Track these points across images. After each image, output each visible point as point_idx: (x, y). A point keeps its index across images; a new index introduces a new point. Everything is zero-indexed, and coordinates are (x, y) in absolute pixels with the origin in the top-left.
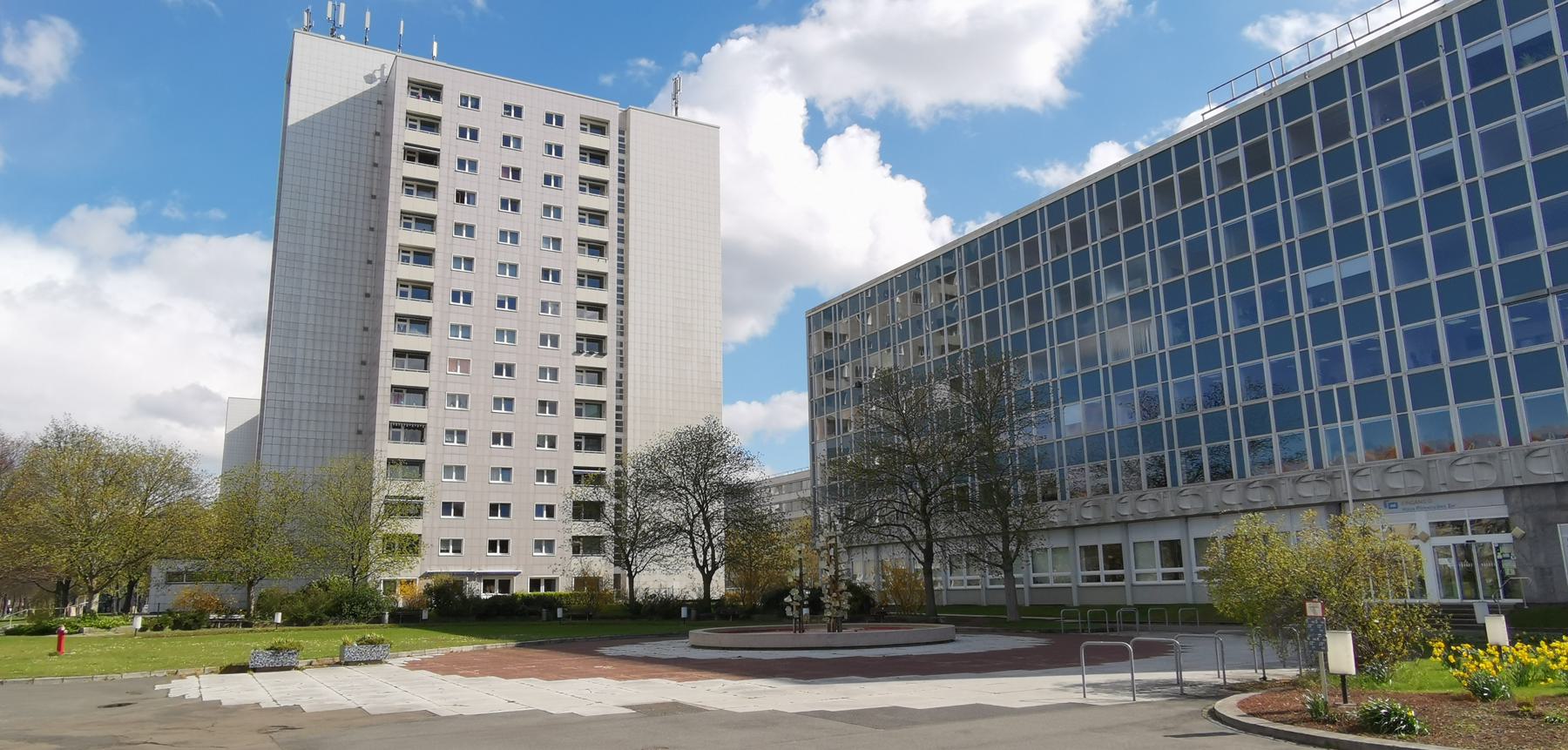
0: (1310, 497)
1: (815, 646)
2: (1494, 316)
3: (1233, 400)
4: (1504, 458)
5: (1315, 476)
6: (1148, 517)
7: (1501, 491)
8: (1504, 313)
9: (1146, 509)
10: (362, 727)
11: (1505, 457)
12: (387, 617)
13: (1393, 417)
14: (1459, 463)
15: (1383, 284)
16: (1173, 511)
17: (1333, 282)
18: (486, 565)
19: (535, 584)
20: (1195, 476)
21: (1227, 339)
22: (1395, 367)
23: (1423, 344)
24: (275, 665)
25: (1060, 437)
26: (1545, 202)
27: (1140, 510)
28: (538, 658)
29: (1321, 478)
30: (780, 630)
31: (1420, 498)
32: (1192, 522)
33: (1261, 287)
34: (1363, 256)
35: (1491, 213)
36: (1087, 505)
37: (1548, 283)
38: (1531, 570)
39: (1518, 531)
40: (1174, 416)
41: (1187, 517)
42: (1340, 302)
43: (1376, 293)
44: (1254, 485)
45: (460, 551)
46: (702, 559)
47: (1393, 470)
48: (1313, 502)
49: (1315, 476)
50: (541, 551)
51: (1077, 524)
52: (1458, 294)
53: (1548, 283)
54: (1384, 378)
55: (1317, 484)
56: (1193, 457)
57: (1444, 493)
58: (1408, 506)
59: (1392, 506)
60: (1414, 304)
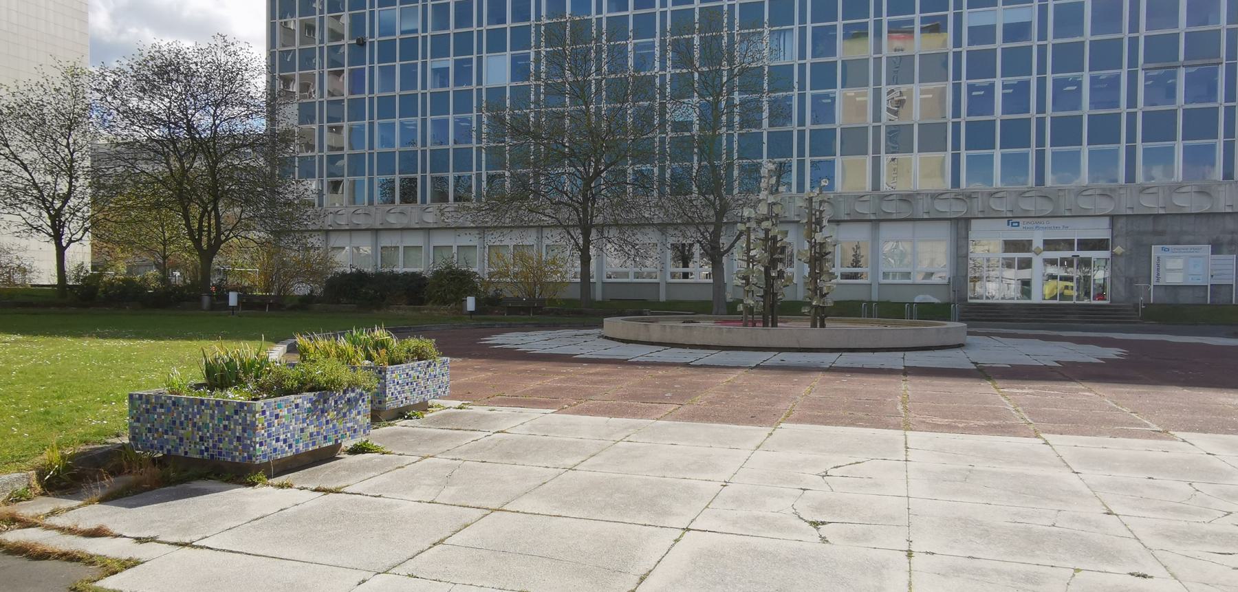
0: (867, 214)
1: (716, 343)
2: (1133, 77)
3: (424, 143)
4: (1121, 192)
5: (954, 194)
6: (395, 227)
7: (947, 225)
8: (1141, 76)
9: (393, 220)
10: (181, 545)
11: (1122, 192)
13: (1032, 152)
14: (1085, 193)
15: (1042, 35)
16: (382, 224)
17: (449, 68)
20: (441, 197)
21: (371, 99)
22: (1041, 108)
23: (1066, 95)
25: (373, 149)
26: (925, 17)
28: (683, 376)
29: (959, 197)
30: (1051, 321)
31: (1040, 220)
33: (455, 60)
34: (503, 55)
36: (358, 212)
37: (1181, 57)
38: (1124, 279)
39: (1118, 250)
40: (429, 147)
42: (999, 45)
43: (1035, 43)
44: (890, 198)
46: (197, 226)
48: (343, 228)
49: (954, 194)
52: (1106, 55)
53: (1181, 57)
54: (835, 127)
55: (954, 202)
56: (440, 182)
57: (1068, 216)
58: (1029, 226)
59: (1014, 224)
60: (1067, 58)
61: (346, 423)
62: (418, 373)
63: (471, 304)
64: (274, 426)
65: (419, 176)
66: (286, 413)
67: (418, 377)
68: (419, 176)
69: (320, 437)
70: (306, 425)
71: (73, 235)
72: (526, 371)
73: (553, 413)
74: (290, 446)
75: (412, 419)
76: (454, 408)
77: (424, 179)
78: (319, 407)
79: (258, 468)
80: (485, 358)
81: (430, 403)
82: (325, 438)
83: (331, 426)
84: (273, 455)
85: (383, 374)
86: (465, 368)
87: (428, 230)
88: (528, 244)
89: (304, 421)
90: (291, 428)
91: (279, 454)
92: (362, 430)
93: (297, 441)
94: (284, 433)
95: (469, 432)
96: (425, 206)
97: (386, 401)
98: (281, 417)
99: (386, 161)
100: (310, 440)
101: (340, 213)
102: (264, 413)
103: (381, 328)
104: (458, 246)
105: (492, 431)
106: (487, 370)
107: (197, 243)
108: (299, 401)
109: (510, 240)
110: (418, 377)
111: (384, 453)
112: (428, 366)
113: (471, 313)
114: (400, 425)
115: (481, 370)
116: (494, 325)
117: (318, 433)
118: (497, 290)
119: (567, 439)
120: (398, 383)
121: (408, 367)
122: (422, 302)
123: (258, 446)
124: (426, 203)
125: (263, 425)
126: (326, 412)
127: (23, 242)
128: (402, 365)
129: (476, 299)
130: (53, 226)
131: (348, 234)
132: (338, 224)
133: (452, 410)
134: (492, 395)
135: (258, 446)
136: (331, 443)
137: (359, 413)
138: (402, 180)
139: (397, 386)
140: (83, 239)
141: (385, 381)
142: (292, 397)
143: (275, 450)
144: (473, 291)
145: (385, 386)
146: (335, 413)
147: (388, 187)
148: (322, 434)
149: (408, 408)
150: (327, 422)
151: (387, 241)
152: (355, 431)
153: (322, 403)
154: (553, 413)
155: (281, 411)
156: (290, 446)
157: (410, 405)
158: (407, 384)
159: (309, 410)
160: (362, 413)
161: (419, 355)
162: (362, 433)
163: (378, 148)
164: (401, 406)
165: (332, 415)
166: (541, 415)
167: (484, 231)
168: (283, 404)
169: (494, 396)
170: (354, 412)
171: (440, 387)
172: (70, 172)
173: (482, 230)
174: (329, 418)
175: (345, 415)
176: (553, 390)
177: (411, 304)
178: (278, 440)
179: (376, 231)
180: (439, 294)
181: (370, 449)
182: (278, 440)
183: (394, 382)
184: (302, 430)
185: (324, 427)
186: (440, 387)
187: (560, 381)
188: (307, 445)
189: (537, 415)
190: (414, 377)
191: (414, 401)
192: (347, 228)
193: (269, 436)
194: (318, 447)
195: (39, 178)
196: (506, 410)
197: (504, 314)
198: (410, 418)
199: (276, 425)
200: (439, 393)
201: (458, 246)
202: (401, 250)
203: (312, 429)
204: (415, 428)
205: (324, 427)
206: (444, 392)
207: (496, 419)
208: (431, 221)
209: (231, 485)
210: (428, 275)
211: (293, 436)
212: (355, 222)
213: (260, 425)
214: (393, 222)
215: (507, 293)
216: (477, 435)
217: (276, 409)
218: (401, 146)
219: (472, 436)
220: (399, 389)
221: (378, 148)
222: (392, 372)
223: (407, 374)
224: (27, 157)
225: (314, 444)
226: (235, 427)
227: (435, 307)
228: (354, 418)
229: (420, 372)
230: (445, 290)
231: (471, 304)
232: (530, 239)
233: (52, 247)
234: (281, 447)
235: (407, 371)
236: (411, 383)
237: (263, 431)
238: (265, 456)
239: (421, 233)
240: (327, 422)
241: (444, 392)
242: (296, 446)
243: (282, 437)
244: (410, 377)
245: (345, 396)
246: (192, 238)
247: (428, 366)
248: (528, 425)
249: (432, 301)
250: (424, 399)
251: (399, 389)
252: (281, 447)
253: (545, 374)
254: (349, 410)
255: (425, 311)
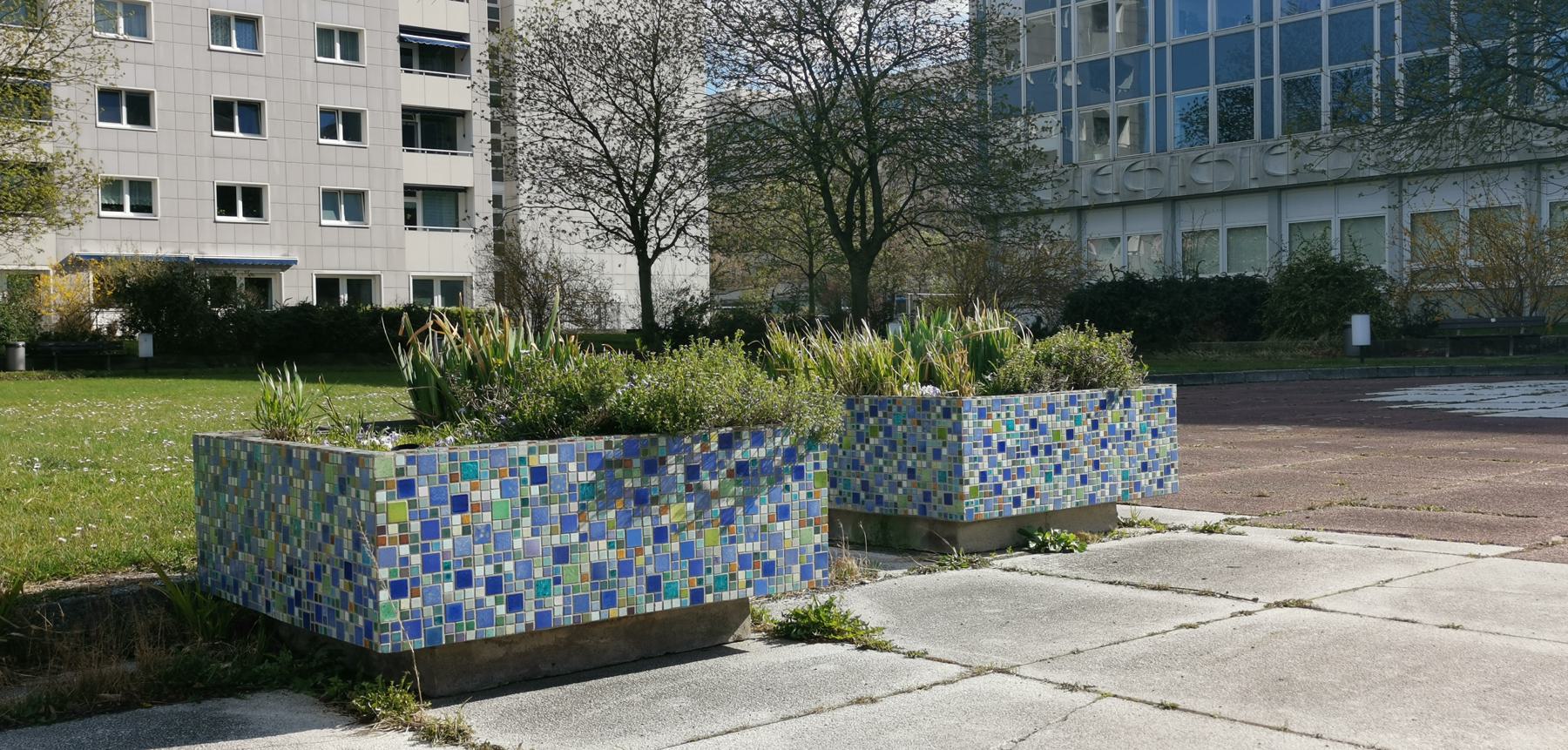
6: (1209, 190)
9: (1206, 177)
12: (21, 353)
18: (216, 244)
19: (327, 286)
20: (1303, 118)
24: (633, 599)
27: (1271, 170)
32: (1284, 194)
35: (469, 46)
36: (1137, 167)
41: (1402, 177)
45: (148, 209)
47: (1203, 160)
50: (338, 218)
51: (1086, 203)
56: (1301, 92)
61: (733, 540)
62: (1068, 424)
63: (1360, 329)
64: (447, 534)
65: (1256, 83)
66: (496, 494)
67: (1070, 434)
68: (1256, 83)
69: (632, 580)
70: (575, 537)
71: (661, 238)
72: (1456, 451)
73: (1502, 556)
74: (515, 603)
75: (1047, 552)
76: (1194, 530)
77: (1267, 86)
78: (628, 483)
79: (397, 664)
80: (1349, 426)
81: (1123, 512)
82: (653, 584)
83: (675, 547)
84: (448, 629)
85: (954, 417)
86: (1288, 445)
87: (1277, 192)
88: (1505, 202)
89: (567, 524)
90: (518, 544)
91: (470, 627)
92: (796, 568)
93: (542, 590)
94: (487, 561)
95: (1187, 599)
96: (1270, 142)
97: (962, 497)
98: (478, 507)
99: (1189, 62)
100: (594, 587)
101: (1103, 172)
102: (407, 488)
103: (990, 306)
104: (1342, 220)
105: (1266, 598)
106: (1348, 449)
107: (844, 238)
108: (547, 459)
109: (1450, 197)
110: (1070, 434)
111: (864, 648)
112: (1103, 405)
113: (1364, 351)
114: (998, 571)
115: (1327, 448)
116: (1413, 370)
117: (625, 569)
118: (1428, 302)
119: (1533, 646)
120: (1002, 447)
121: (1038, 404)
122: (1256, 333)
123: (384, 595)
124: (1271, 136)
125: (403, 527)
126: (655, 500)
127: (595, 256)
128: (1017, 396)
129: (1373, 324)
130: (633, 227)
131: (1118, 212)
132: (1100, 194)
133: (1183, 535)
134: (1326, 498)
135: (384, 595)
136: (676, 603)
137: (783, 513)
138: (1222, 95)
139: (1000, 456)
140: (676, 244)
141: (960, 439)
142: (521, 447)
143: (455, 612)
144: (1370, 304)
145: (960, 453)
146: (691, 506)
147: (1194, 122)
148: (640, 571)
149: (1046, 520)
150: (660, 535)
151: (1190, 219)
152: (769, 569)
153: (636, 473)
154: (1502, 556)
155: (474, 488)
156: (515, 603)
157: (1047, 513)
158: (1034, 451)
159: (589, 490)
160: (795, 513)
161: (1079, 376)
162: (797, 577)
163: (1173, 37)
164: (1015, 512)
165: (677, 511)
166: (1464, 560)
167: (1401, 184)
168: (484, 466)
169: (1330, 505)
170: (764, 509)
171: (1144, 467)
172: (656, 128)
173: (1396, 179)
174: (665, 520)
175: (727, 518)
176: (1523, 494)
177: (1235, 339)
178: (464, 580)
179: (1171, 203)
180: (1294, 314)
181: (831, 630)
182: (464, 580)
183: (988, 441)
184: (561, 555)
185: (648, 550)
186: (1144, 467)
187: (1553, 475)
188: (582, 604)
189: (1443, 561)
190: (1057, 434)
191: (1056, 502)
192: (1116, 200)
193: (430, 564)
194: (623, 612)
195: (612, 144)
196: (1346, 542)
197: (1443, 354)
198: (1042, 548)
199: (457, 531)
200: (1144, 483)
201: (1342, 220)
202: (1223, 235)
203: (599, 551)
204: (1038, 579)
205: (648, 550)
206: (1160, 483)
207: (1306, 564)
208: (1285, 173)
209: (333, 715)
210: (1268, 274)
211: (525, 570)
212: (1131, 187)
213: (393, 530)
214: (1207, 181)
215: (1453, 310)
216: (1212, 610)
217: (454, 478)
218: (1218, 27)
219: (1179, 610)
220: (1006, 464)
221: (1173, 37)
222: (982, 414)
223: (1033, 423)
224: (596, 113)
225: (608, 600)
226: (341, 532)
227: (1286, 341)
228: (764, 528)
229: (1078, 421)
230: (1306, 307)
231: (1360, 329)
232: (1507, 192)
233: (633, 261)
234: (479, 603)
235: (1033, 413)
236: (1048, 450)
237: (404, 550)
238: (414, 629)
239: (1263, 200)
240: (660, 535)
241: (1160, 483)
242: (538, 604)
243: (480, 571)
244: (1043, 431)
245: (729, 456)
246: (836, 231)
247: (1103, 405)
248: (1399, 589)
249: (1277, 331)
250: (1092, 497)
251: (1006, 464)
252: (479, 603)
253: (1510, 459)
254: (747, 502)
255: (1265, 353)
